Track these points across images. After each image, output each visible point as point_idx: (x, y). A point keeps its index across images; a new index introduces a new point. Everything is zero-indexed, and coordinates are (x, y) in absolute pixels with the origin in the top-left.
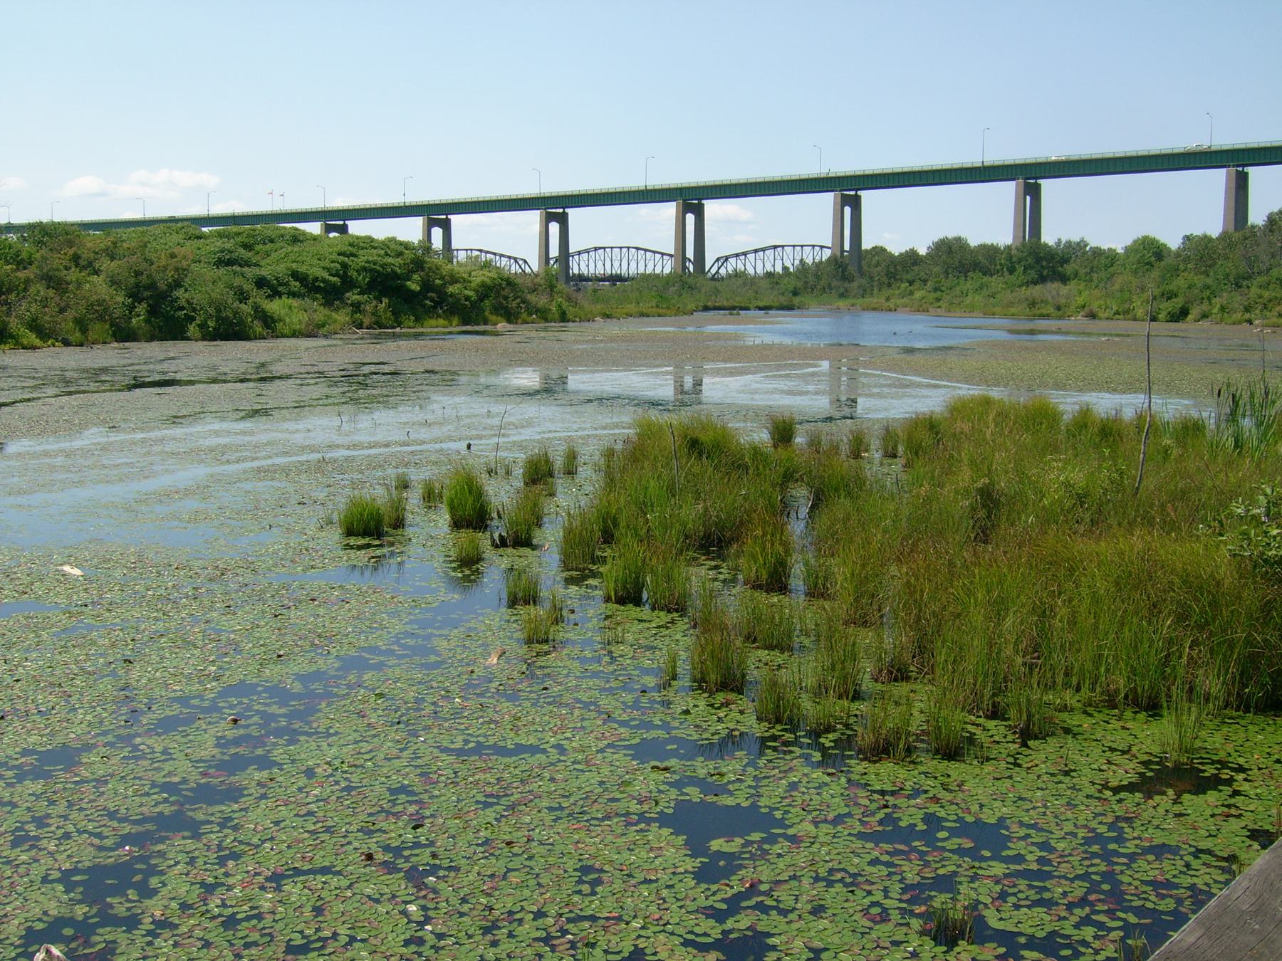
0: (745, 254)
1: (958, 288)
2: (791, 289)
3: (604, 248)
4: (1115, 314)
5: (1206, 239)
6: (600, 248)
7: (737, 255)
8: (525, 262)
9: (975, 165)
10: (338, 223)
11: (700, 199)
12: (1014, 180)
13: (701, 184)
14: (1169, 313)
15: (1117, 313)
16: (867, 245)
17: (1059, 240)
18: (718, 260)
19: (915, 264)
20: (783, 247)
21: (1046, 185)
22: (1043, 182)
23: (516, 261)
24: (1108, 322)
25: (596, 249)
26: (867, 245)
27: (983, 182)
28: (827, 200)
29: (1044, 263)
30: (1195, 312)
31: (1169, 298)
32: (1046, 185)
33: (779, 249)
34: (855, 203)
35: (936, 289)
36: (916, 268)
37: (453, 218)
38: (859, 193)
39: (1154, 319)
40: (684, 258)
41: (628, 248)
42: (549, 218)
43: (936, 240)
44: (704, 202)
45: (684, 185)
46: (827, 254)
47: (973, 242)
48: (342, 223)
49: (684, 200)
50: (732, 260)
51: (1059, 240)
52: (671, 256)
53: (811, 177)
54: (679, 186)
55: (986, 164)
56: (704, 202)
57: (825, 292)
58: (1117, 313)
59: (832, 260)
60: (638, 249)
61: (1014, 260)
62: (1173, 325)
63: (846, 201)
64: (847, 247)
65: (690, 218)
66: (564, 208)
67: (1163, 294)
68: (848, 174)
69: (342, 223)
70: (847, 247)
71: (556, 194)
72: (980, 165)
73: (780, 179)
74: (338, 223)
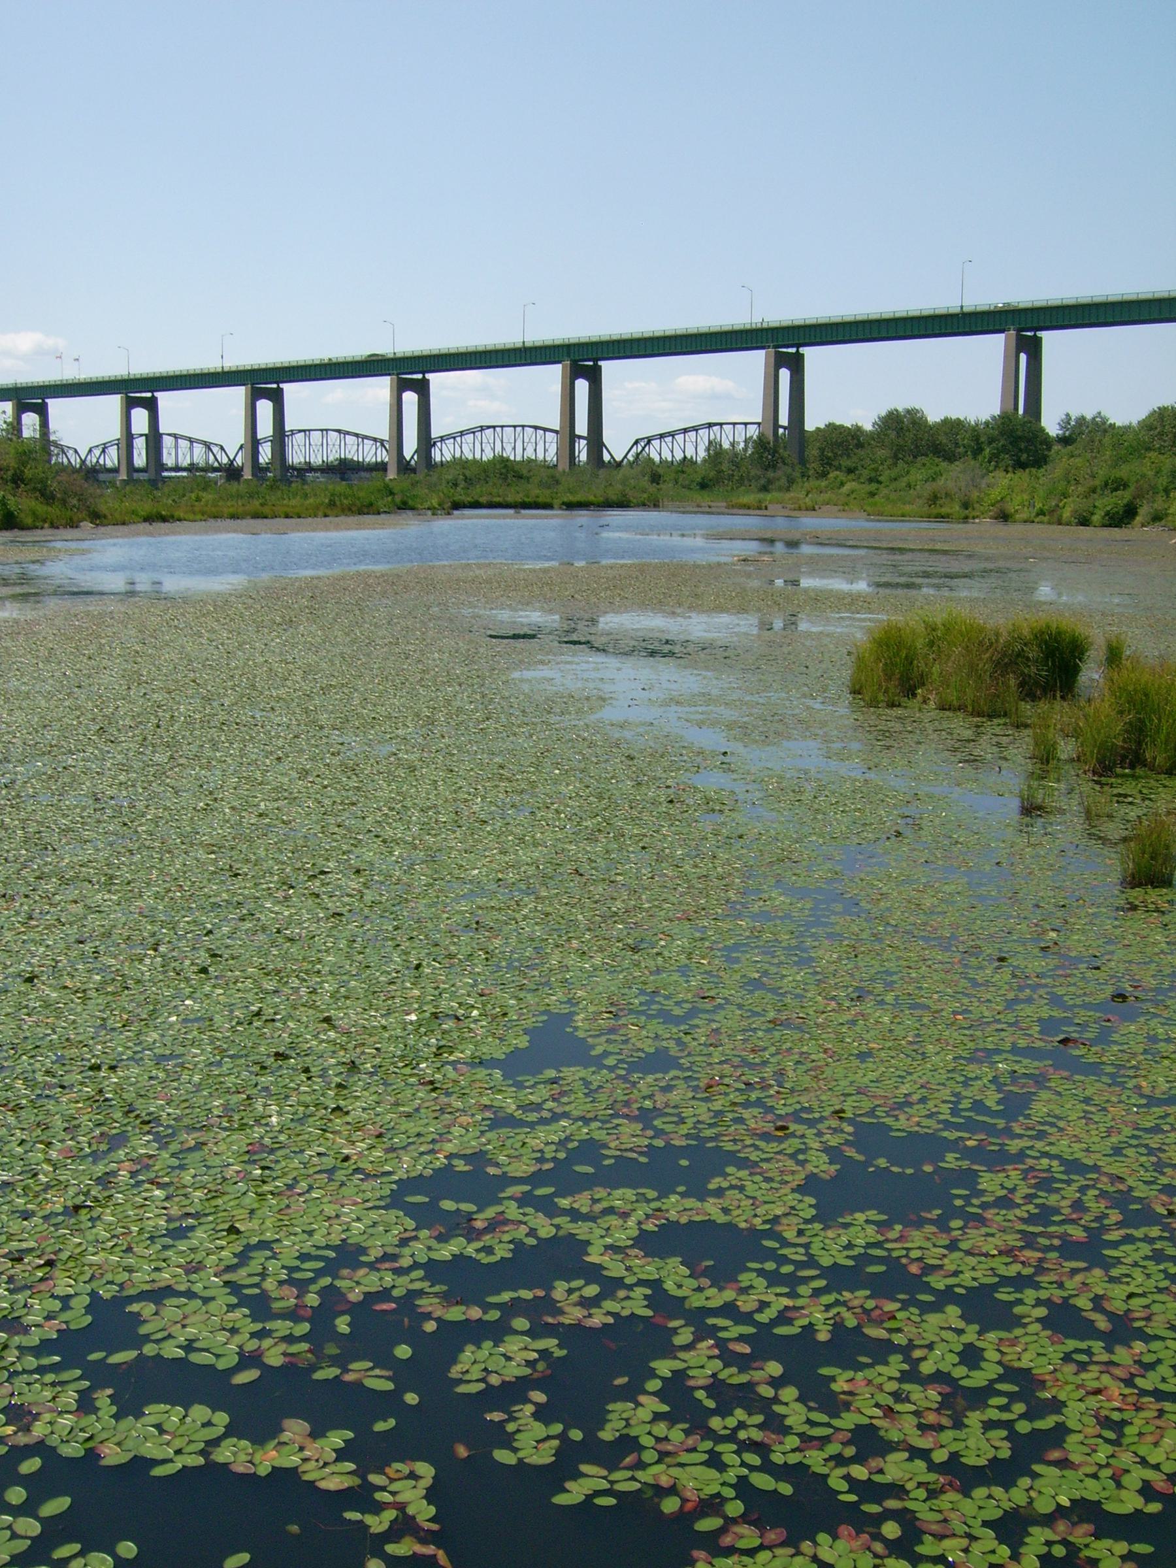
0: (672, 434)
1: (905, 479)
2: (699, 480)
3: (494, 427)
4: (1038, 515)
5: (858, 429)
6: (489, 427)
7: (662, 436)
8: (222, 448)
9: (952, 311)
10: (144, 395)
11: (596, 360)
12: (763, 348)
13: (646, 335)
14: (1107, 513)
15: (1041, 513)
16: (813, 421)
17: (1068, 415)
18: (636, 442)
19: (860, 445)
20: (721, 424)
21: (1049, 338)
22: (1045, 335)
23: (383, 445)
24: (1029, 526)
25: (482, 429)
26: (813, 421)
27: (684, 353)
28: (756, 361)
29: (1023, 445)
30: (1144, 512)
31: (1116, 489)
32: (1049, 338)
33: (716, 428)
34: (796, 365)
35: (871, 480)
36: (860, 452)
37: (287, 387)
38: (802, 350)
39: (1084, 522)
40: (573, 437)
41: (523, 426)
42: (402, 386)
43: (883, 413)
44: (601, 363)
45: (572, 341)
46: (753, 431)
47: (934, 416)
48: (149, 395)
49: (1019, 330)
50: (656, 443)
51: (1068, 415)
52: (556, 432)
53: (979, 309)
54: (567, 342)
55: (965, 310)
56: (601, 363)
57: (742, 484)
58: (1041, 513)
59: (761, 444)
60: (536, 428)
61: (982, 439)
62: (1116, 533)
63: (780, 361)
64: (784, 420)
65: (582, 386)
66: (798, 346)
67: (1106, 484)
68: (636, 336)
69: (149, 395)
70: (784, 420)
71: (660, 334)
72: (958, 310)
73: (587, 340)
74: (144, 395)
